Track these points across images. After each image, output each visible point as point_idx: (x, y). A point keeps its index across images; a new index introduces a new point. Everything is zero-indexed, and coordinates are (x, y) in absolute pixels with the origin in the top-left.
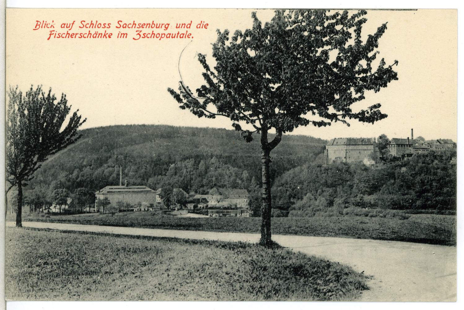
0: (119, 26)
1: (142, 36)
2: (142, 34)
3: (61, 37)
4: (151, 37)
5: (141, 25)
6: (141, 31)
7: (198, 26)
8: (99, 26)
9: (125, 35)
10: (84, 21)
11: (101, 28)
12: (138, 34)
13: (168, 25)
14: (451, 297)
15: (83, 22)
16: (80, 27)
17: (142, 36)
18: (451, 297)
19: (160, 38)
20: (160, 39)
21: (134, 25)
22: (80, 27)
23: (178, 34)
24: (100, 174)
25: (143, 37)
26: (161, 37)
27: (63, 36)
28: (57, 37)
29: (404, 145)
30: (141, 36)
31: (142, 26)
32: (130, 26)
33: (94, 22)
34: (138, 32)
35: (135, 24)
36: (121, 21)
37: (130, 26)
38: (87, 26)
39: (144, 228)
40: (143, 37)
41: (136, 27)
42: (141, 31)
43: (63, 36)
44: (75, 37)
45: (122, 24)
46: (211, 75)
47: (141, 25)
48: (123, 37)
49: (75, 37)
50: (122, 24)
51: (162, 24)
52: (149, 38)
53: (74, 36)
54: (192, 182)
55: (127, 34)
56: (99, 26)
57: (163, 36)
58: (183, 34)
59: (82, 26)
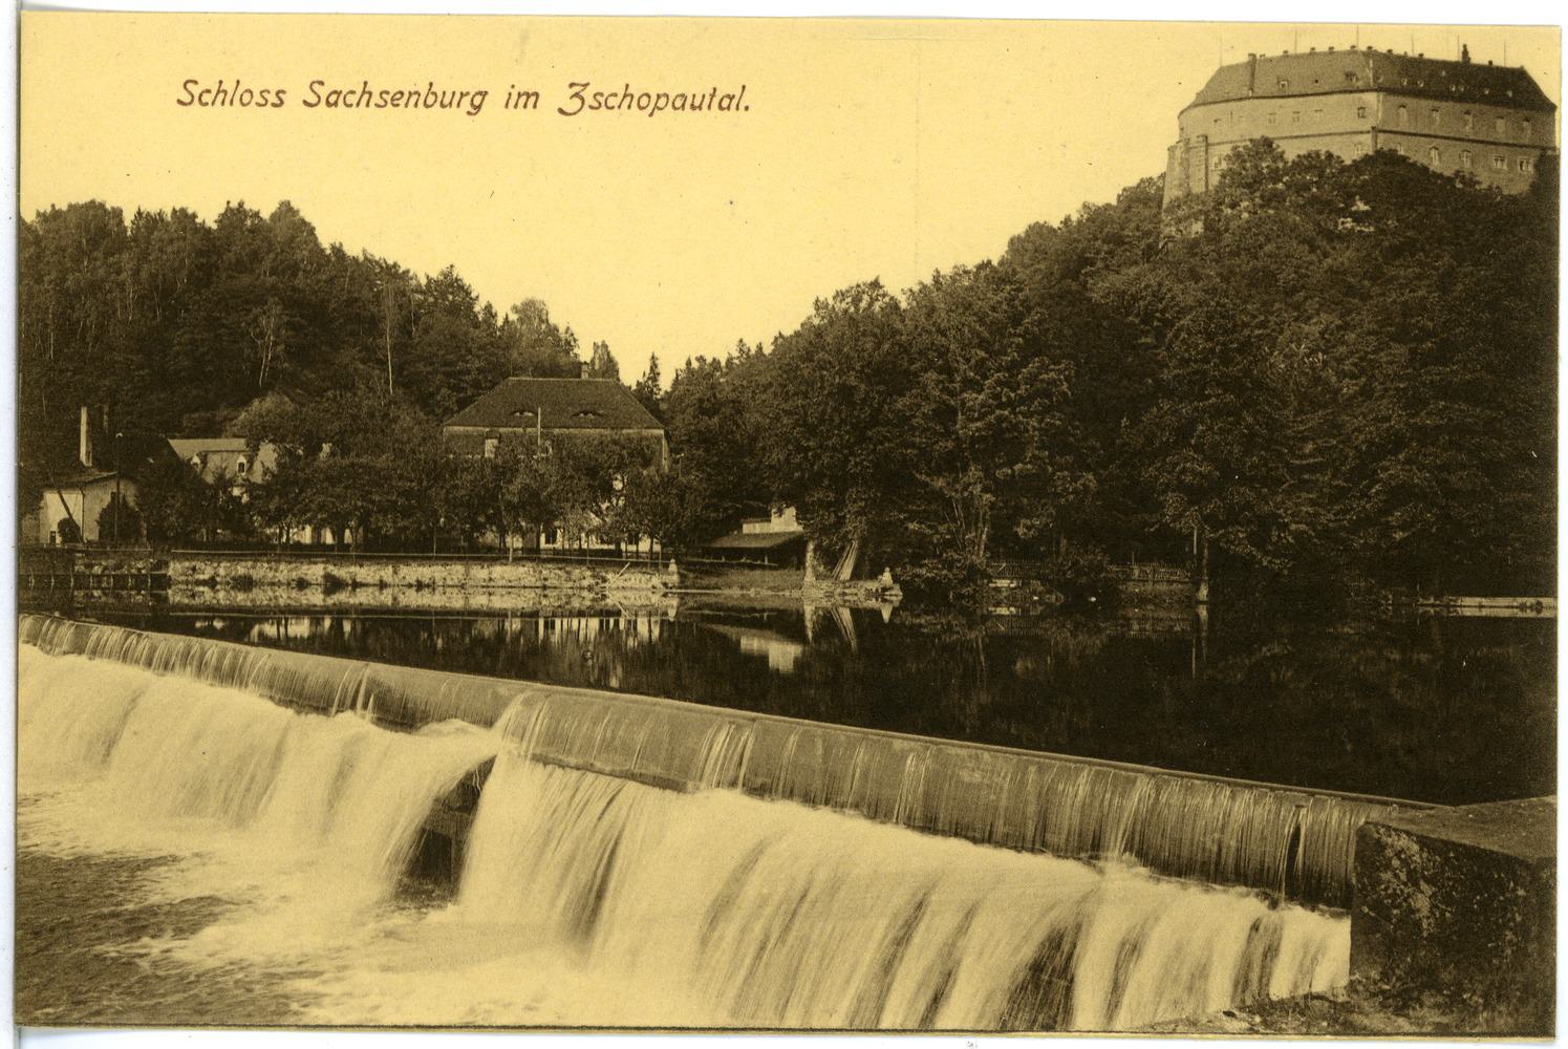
0: (187, 99)
2: (588, 94)
4: (358, 104)
5: (602, 100)
8: (247, 97)
9: (533, 99)
12: (576, 95)
13: (484, 94)
14: (1543, 1027)
16: (180, 102)
17: (589, 101)
18: (1543, 1027)
19: (650, 109)
20: (651, 115)
21: (366, 96)
22: (180, 102)
23: (713, 96)
25: (591, 107)
26: (656, 107)
27: (204, 99)
28: (378, 106)
31: (392, 100)
32: (352, 99)
33: (229, 86)
34: (576, 89)
37: (352, 99)
39: (385, 728)
40: (591, 107)
41: (372, 103)
45: (323, 92)
46: (328, 577)
47: (602, 100)
48: (525, 106)
55: (537, 95)
56: (247, 97)
57: (662, 102)
58: (731, 98)
59: (313, 99)
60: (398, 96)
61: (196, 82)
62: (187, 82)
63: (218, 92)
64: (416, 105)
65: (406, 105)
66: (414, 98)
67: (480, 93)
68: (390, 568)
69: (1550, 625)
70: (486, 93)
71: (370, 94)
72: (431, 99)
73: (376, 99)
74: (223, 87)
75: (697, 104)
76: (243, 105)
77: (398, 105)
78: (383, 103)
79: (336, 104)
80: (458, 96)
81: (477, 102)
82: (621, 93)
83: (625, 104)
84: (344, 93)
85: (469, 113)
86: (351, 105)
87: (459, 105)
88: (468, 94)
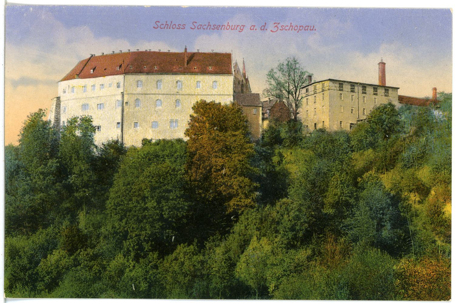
0: (156, 26)
2: (279, 26)
3: (159, 28)
4: (289, 30)
5: (283, 27)
6: (279, 23)
7: (252, 28)
8: (296, 28)
10: (159, 22)
11: (176, 29)
12: (276, 26)
13: (244, 26)
15: (157, 23)
16: (191, 28)
17: (280, 28)
19: (298, 30)
20: (298, 32)
21: (209, 27)
24: (82, 232)
25: (280, 30)
26: (299, 30)
27: (161, 27)
29: (364, 86)
30: (279, 29)
31: (217, 27)
33: (169, 23)
34: (276, 25)
35: (211, 26)
37: (205, 27)
42: (279, 23)
43: (161, 27)
45: (196, 25)
50: (196, 25)
51: (237, 26)
54: (394, 294)
56: (174, 26)
60: (218, 26)
61: (196, 23)
62: (157, 22)
63: (291, 26)
64: (292, 30)
65: (221, 29)
68: (191, 245)
69: (9, 231)
70: (255, 26)
74: (292, 25)
76: (173, 28)
77: (218, 29)
78: (214, 28)
79: (200, 28)
80: (236, 26)
81: (242, 28)
83: (290, 29)
84: (203, 25)
85: (239, 31)
86: (205, 29)
87: (236, 29)
88: (239, 26)
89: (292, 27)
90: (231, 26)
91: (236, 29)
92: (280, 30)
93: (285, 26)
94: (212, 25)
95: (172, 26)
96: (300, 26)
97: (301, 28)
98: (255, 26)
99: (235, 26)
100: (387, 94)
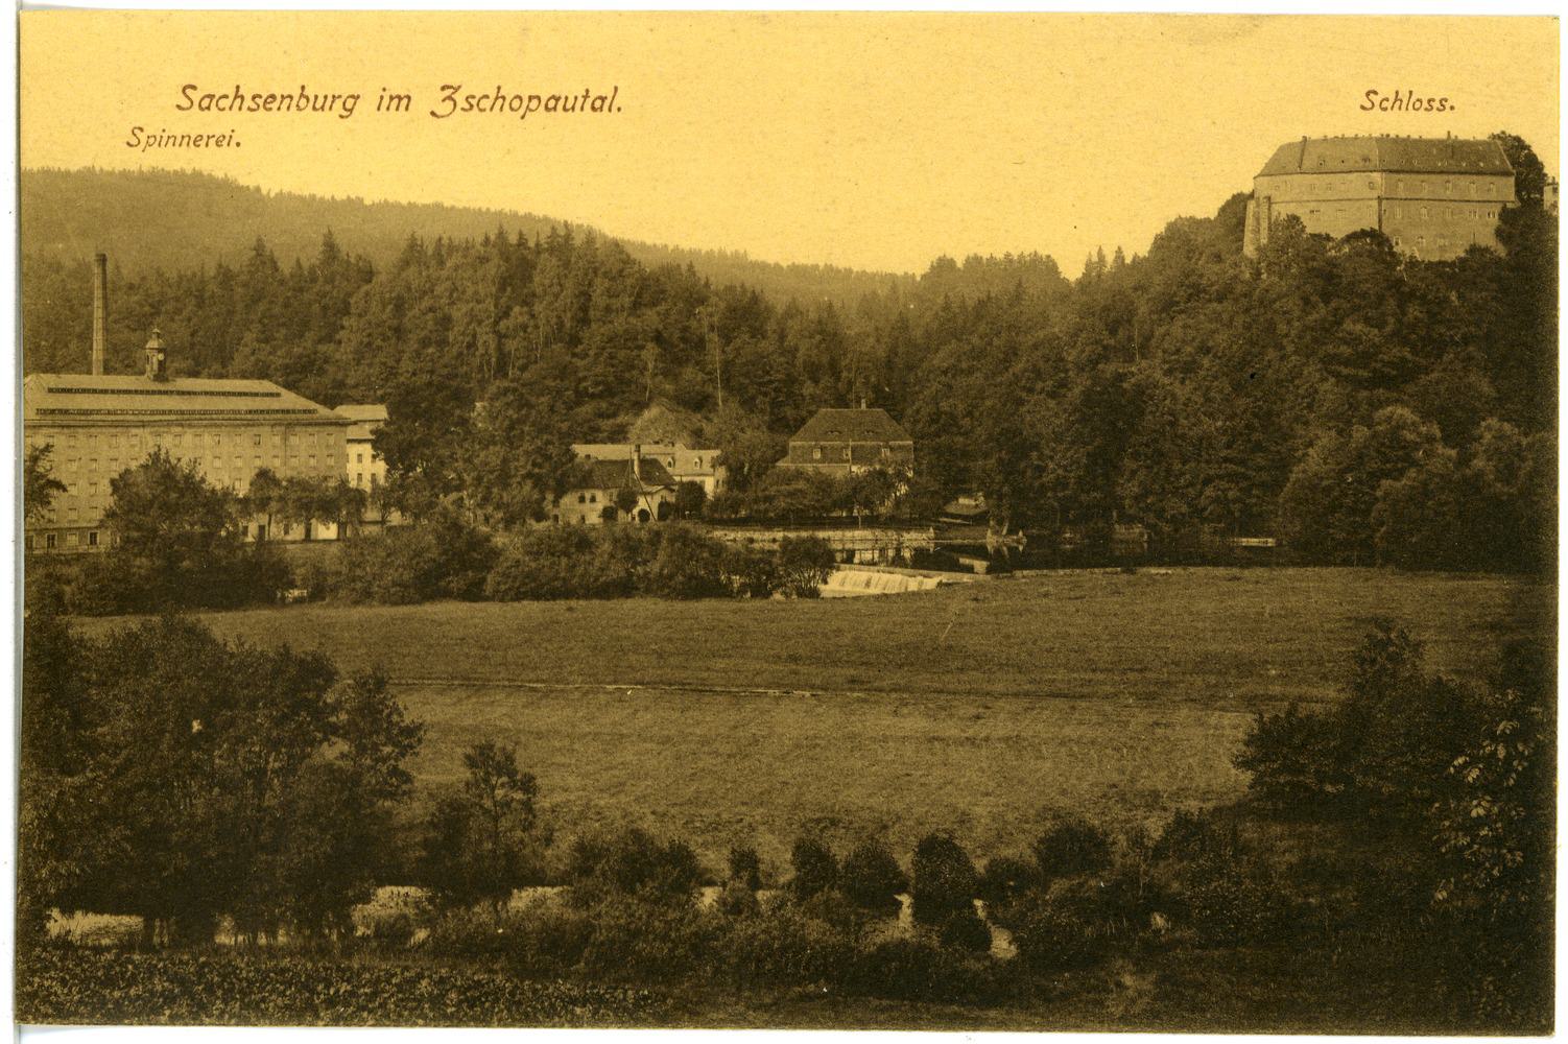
0: (255, 106)
1: (462, 103)
2: (460, 97)
4: (231, 108)
5: (474, 102)
8: (1418, 105)
9: (405, 101)
12: (450, 98)
14: (1545, 1027)
15: (1372, 96)
17: (462, 103)
18: (1545, 1027)
19: (521, 112)
20: (523, 117)
23: (586, 97)
28: (249, 109)
33: (1404, 96)
34: (448, 92)
36: (194, 87)
37: (224, 103)
38: (1385, 104)
44: (207, 145)
45: (196, 96)
47: (260, 101)
49: (207, 145)
52: (1385, 109)
53: (203, 143)
55: (409, 98)
56: (1418, 105)
58: (603, 99)
59: (185, 103)
63: (497, 98)
66: (569, 106)
67: (352, 97)
70: (358, 97)
71: (242, 98)
72: (304, 101)
73: (248, 102)
74: (502, 93)
75: (318, 106)
79: (208, 108)
80: (330, 99)
81: (348, 106)
82: (232, 94)
88: (340, 97)
89: (501, 100)
90: (312, 99)
91: (331, 108)
92: (463, 109)
93: (264, 97)
94: (248, 98)
95: (589, 101)
96: (530, 98)
97: (534, 103)
98: (358, 97)
99: (326, 97)
100: (97, 355)
